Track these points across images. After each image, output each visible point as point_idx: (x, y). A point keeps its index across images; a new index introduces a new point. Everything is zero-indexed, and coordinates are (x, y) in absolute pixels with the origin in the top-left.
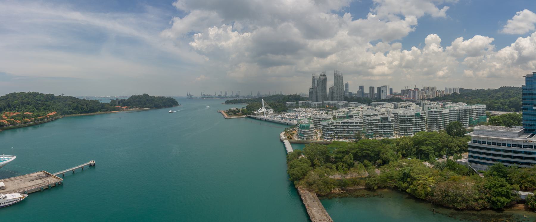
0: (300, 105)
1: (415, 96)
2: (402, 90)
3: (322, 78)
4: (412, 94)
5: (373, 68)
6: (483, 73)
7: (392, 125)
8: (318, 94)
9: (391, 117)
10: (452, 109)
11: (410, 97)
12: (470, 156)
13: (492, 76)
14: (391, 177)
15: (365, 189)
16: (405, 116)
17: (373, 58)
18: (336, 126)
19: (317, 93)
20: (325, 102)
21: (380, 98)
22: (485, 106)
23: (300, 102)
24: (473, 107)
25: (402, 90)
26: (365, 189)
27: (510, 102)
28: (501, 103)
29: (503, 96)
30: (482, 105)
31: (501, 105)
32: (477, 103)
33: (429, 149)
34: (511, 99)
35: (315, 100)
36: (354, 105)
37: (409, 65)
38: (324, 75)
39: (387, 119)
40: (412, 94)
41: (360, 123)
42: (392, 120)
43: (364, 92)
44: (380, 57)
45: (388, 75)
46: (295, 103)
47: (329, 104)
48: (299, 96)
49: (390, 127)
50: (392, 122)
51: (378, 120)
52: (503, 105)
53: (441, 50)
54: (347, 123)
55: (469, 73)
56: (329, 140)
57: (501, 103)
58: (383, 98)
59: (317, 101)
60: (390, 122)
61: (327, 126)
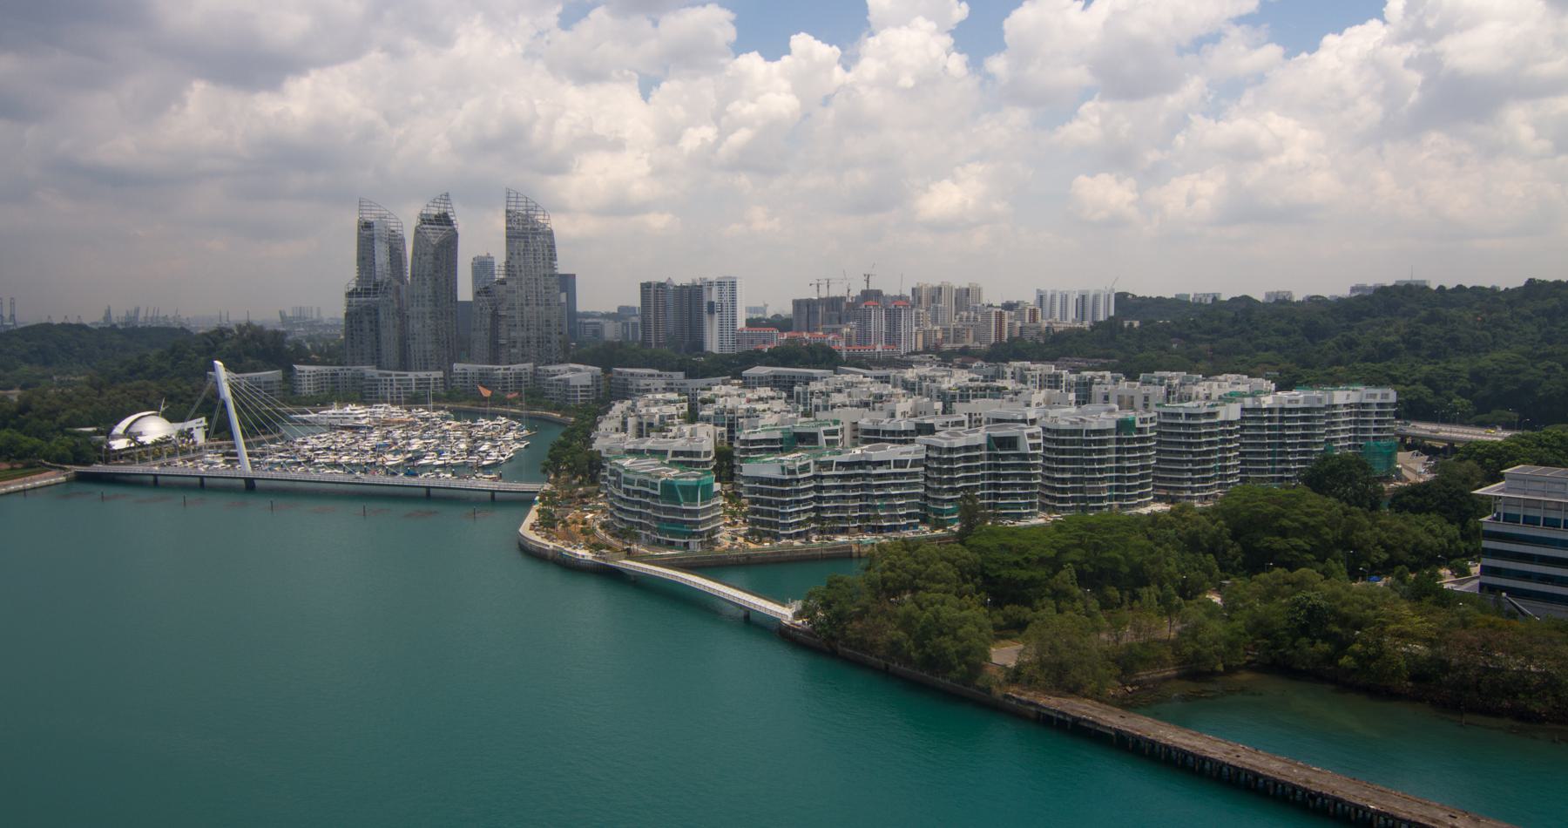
0: (307, 388)
1: (892, 338)
2: (797, 304)
3: (434, 235)
4: (878, 323)
5: (559, 167)
6: (1196, 193)
7: (1035, 466)
8: (415, 326)
9: (1028, 438)
10: (1249, 402)
11: (864, 337)
12: (1485, 570)
13: (1246, 212)
14: (1260, 628)
15: (1178, 677)
16: (1075, 432)
17: (578, 107)
18: (815, 477)
19: (402, 315)
20: (457, 367)
21: (698, 345)
22: (1392, 397)
23: (304, 369)
24: (1340, 396)
25: (797, 304)
26: (1178, 677)
27: (1478, 377)
28: (1428, 382)
29: (1413, 345)
30: (1378, 391)
31: (1425, 391)
32: (1348, 382)
33: (1294, 548)
34: (1485, 361)
35: (390, 349)
36: (661, 383)
37: (768, 155)
38: (444, 220)
39: (1011, 442)
40: (878, 323)
41: (915, 463)
42: (1033, 447)
43: (581, 307)
44: (623, 109)
45: (644, 208)
46: (273, 375)
47: (486, 380)
48: (278, 336)
49: (996, 486)
50: (1034, 456)
51: (978, 447)
52: (1437, 392)
53: (956, 63)
54: (860, 464)
55: (1108, 192)
56: (797, 543)
57: (1428, 382)
58: (713, 342)
59: (404, 365)
60: (1024, 456)
61: (782, 482)
